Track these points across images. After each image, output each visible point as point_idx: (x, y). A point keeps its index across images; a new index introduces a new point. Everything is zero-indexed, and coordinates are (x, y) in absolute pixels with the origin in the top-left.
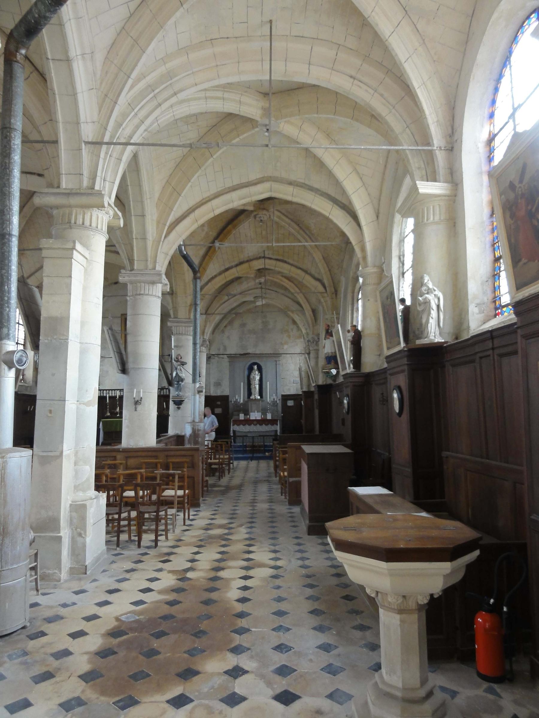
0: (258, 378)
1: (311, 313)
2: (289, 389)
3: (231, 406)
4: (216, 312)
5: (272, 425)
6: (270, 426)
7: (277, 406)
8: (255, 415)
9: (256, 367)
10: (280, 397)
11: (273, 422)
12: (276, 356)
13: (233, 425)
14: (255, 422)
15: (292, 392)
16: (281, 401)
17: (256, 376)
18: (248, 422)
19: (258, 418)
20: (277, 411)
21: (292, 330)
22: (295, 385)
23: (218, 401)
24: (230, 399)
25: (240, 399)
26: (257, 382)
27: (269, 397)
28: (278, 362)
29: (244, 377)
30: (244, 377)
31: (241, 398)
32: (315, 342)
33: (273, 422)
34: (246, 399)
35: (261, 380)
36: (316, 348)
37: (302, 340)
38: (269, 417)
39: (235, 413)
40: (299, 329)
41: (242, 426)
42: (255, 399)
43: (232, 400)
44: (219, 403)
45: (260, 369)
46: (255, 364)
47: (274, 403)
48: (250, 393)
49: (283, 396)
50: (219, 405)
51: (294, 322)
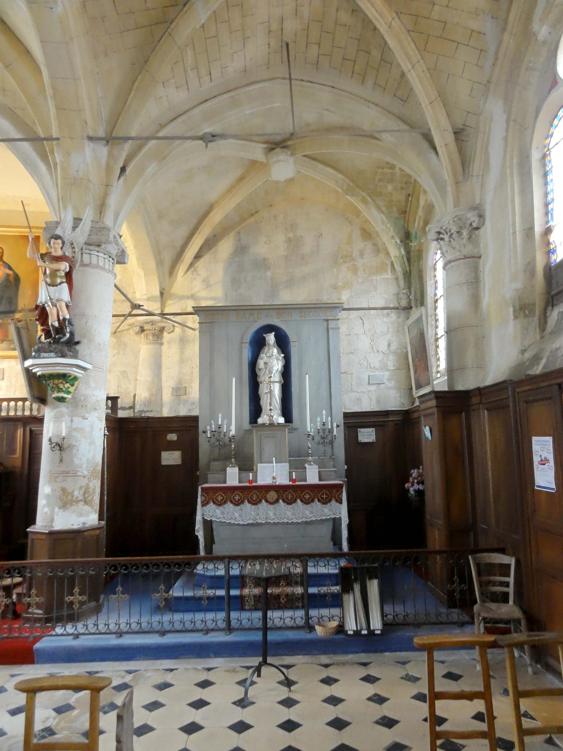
0: (277, 365)
1: (450, 138)
2: (359, 400)
3: (204, 447)
4: (160, 135)
5: (325, 502)
6: (317, 504)
7: (331, 443)
8: (272, 472)
9: (271, 338)
10: (339, 419)
11: (323, 493)
12: (326, 311)
13: (204, 504)
14: (272, 495)
15: (367, 405)
16: (342, 427)
17: (272, 362)
18: (254, 494)
19: (279, 482)
20: (332, 457)
21: (362, 255)
22: (373, 388)
23: (172, 432)
24: (201, 428)
25: (229, 424)
26: (277, 377)
27: (312, 416)
28: (332, 324)
29: (241, 364)
30: (241, 364)
31: (230, 419)
32: (465, 233)
33: (323, 493)
34: (246, 425)
35: (286, 373)
36: (469, 250)
37: (389, 275)
38: (312, 476)
39: (215, 465)
40: (378, 249)
41: (229, 506)
42: (272, 425)
43: (206, 427)
44: (173, 437)
45: (283, 343)
46: (269, 328)
47: (325, 436)
48: (256, 410)
49: (347, 415)
50: (171, 442)
51: (367, 234)
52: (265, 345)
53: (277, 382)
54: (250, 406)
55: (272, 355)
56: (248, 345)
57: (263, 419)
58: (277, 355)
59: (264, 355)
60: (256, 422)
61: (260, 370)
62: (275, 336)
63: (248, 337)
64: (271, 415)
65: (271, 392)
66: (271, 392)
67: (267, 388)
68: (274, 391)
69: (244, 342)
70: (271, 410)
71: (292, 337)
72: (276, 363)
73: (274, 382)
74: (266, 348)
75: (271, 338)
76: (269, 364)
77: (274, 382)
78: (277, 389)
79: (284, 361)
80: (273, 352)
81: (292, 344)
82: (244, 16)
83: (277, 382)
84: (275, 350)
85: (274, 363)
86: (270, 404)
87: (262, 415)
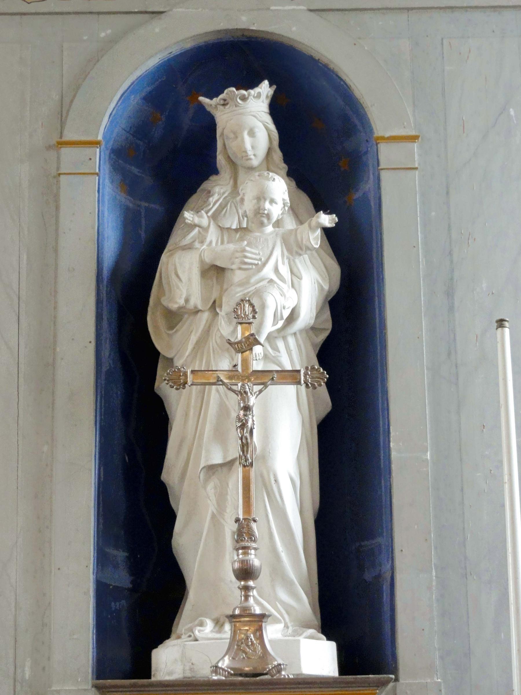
0: (294, 287)
9: (248, 119)
17: (257, 261)
45: (326, 149)
46: (239, 58)
52: (210, 169)
53: (291, 377)
54: (102, 559)
55: (260, 216)
56: (97, 159)
57: (191, 650)
58: (290, 224)
59: (204, 220)
60: (142, 668)
61: (174, 318)
62: (276, 109)
63: (105, 108)
64: (246, 612)
65: (252, 461)
66: (252, 461)
67: (220, 435)
68: (265, 458)
69: (70, 135)
70: (245, 573)
71: (386, 108)
72: (285, 270)
73: (266, 378)
74: (218, 189)
75: (248, 119)
76: (238, 276)
77: (266, 378)
78: (286, 429)
79: (336, 269)
80: (261, 197)
81: (387, 155)
82: (238, 415)
83: (291, 377)
84: (279, 188)
85: (268, 271)
86: (244, 533)
87: (183, 622)
